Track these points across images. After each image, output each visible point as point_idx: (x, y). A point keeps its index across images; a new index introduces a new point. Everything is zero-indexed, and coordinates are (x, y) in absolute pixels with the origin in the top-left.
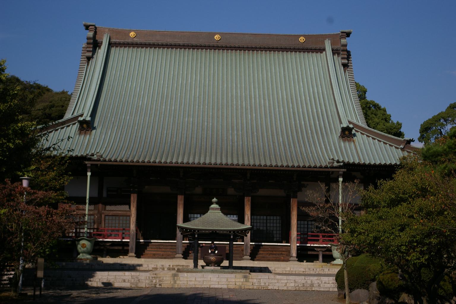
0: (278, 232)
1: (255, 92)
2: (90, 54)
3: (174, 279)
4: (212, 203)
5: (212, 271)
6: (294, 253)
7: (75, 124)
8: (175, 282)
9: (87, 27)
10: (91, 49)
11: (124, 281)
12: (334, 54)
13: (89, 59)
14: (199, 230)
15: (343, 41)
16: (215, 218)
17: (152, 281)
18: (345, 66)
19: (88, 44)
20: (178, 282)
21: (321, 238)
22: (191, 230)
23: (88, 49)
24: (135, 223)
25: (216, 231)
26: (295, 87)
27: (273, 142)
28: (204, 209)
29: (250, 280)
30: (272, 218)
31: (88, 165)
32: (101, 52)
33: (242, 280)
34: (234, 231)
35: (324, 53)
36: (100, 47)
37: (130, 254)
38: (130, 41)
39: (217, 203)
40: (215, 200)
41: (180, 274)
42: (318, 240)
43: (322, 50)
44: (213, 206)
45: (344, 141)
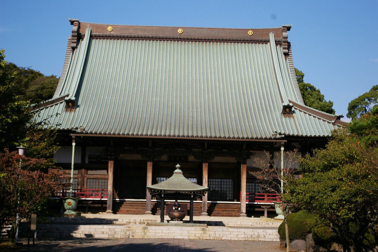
2: (75, 45)
4: (176, 169)
5: (176, 225)
7: (62, 103)
10: (76, 41)
11: (103, 233)
12: (277, 45)
13: (74, 49)
14: (165, 191)
15: (285, 34)
16: (178, 181)
17: (126, 233)
18: (286, 54)
19: (73, 36)
20: (147, 234)
22: (158, 190)
23: (73, 41)
25: (179, 191)
29: (207, 232)
31: (73, 137)
32: (84, 43)
33: (201, 232)
34: (194, 192)
35: (269, 44)
36: (83, 39)
38: (108, 34)
39: (180, 168)
40: (178, 166)
42: (263, 199)
43: (267, 42)
44: (176, 171)
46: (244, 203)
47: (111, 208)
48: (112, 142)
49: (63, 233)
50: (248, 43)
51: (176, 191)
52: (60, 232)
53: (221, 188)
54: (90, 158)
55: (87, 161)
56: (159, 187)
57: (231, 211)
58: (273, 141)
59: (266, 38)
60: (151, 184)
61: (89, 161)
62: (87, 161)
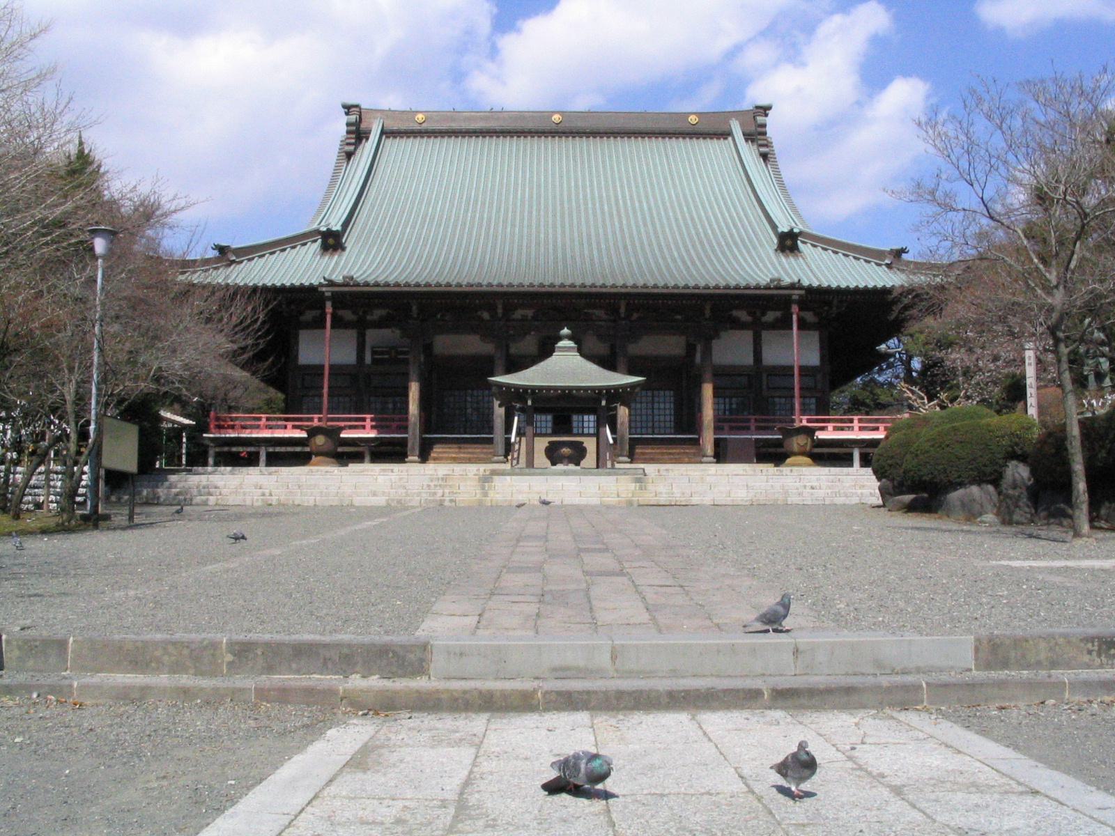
0: (668, 418)
1: (623, 192)
2: (352, 148)
3: (483, 488)
4: (560, 338)
5: (565, 473)
6: (709, 449)
7: (315, 241)
8: (486, 495)
9: (348, 108)
10: (353, 141)
11: (375, 494)
12: (747, 140)
13: (349, 155)
14: (533, 389)
15: (760, 119)
16: (566, 367)
17: (435, 494)
18: (765, 157)
19: (348, 132)
20: (491, 494)
21: (753, 426)
22: (517, 387)
23: (348, 141)
24: (417, 402)
25: (571, 389)
26: (689, 185)
27: (677, 220)
28: (546, 351)
29: (650, 487)
30: (662, 393)
31: (327, 294)
32: (368, 147)
33: (632, 486)
34: (608, 389)
35: (730, 139)
36: (367, 139)
37: (410, 458)
38: (417, 127)
39: (570, 338)
40: (566, 331)
41: (496, 478)
42: (748, 428)
43: (725, 134)
44: (561, 344)
45: (787, 256)
46: (708, 438)
47: (417, 452)
48: (414, 308)
49: (271, 495)
50: (691, 138)
51: (563, 389)
52: (263, 495)
53: (653, 408)
54: (374, 353)
55: (368, 359)
56: (520, 380)
57: (678, 454)
58: (775, 292)
59: (724, 128)
60: (545, 781)
61: (375, 361)
62: (368, 359)
